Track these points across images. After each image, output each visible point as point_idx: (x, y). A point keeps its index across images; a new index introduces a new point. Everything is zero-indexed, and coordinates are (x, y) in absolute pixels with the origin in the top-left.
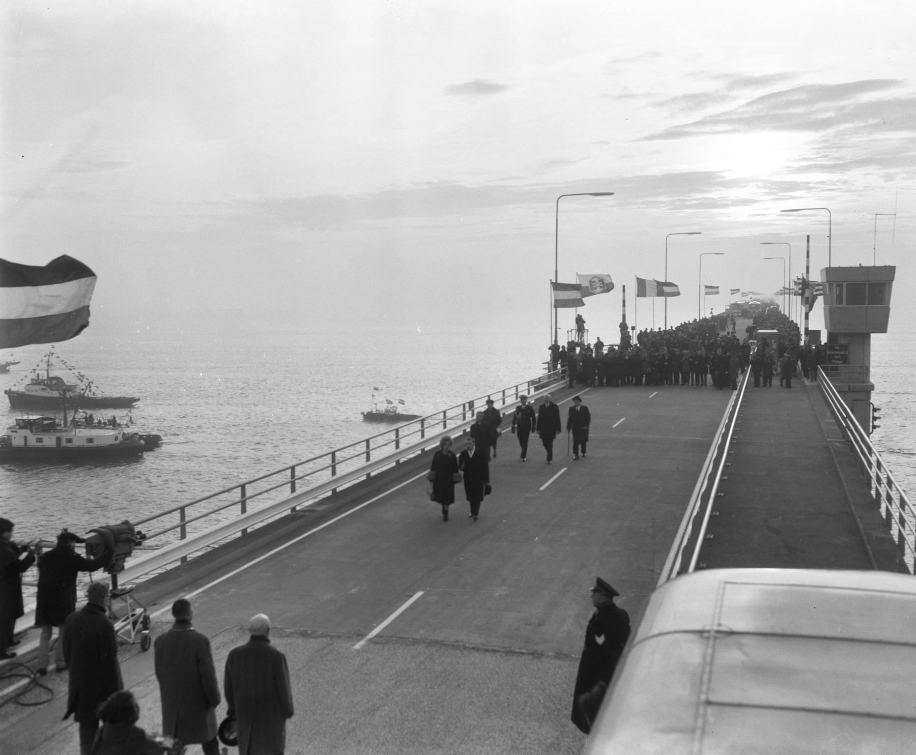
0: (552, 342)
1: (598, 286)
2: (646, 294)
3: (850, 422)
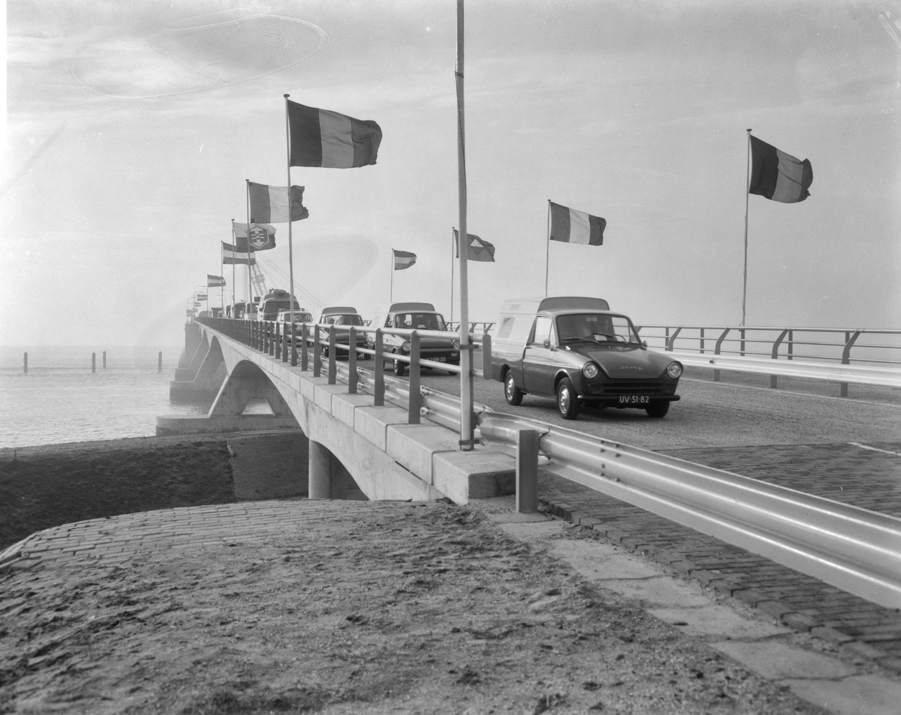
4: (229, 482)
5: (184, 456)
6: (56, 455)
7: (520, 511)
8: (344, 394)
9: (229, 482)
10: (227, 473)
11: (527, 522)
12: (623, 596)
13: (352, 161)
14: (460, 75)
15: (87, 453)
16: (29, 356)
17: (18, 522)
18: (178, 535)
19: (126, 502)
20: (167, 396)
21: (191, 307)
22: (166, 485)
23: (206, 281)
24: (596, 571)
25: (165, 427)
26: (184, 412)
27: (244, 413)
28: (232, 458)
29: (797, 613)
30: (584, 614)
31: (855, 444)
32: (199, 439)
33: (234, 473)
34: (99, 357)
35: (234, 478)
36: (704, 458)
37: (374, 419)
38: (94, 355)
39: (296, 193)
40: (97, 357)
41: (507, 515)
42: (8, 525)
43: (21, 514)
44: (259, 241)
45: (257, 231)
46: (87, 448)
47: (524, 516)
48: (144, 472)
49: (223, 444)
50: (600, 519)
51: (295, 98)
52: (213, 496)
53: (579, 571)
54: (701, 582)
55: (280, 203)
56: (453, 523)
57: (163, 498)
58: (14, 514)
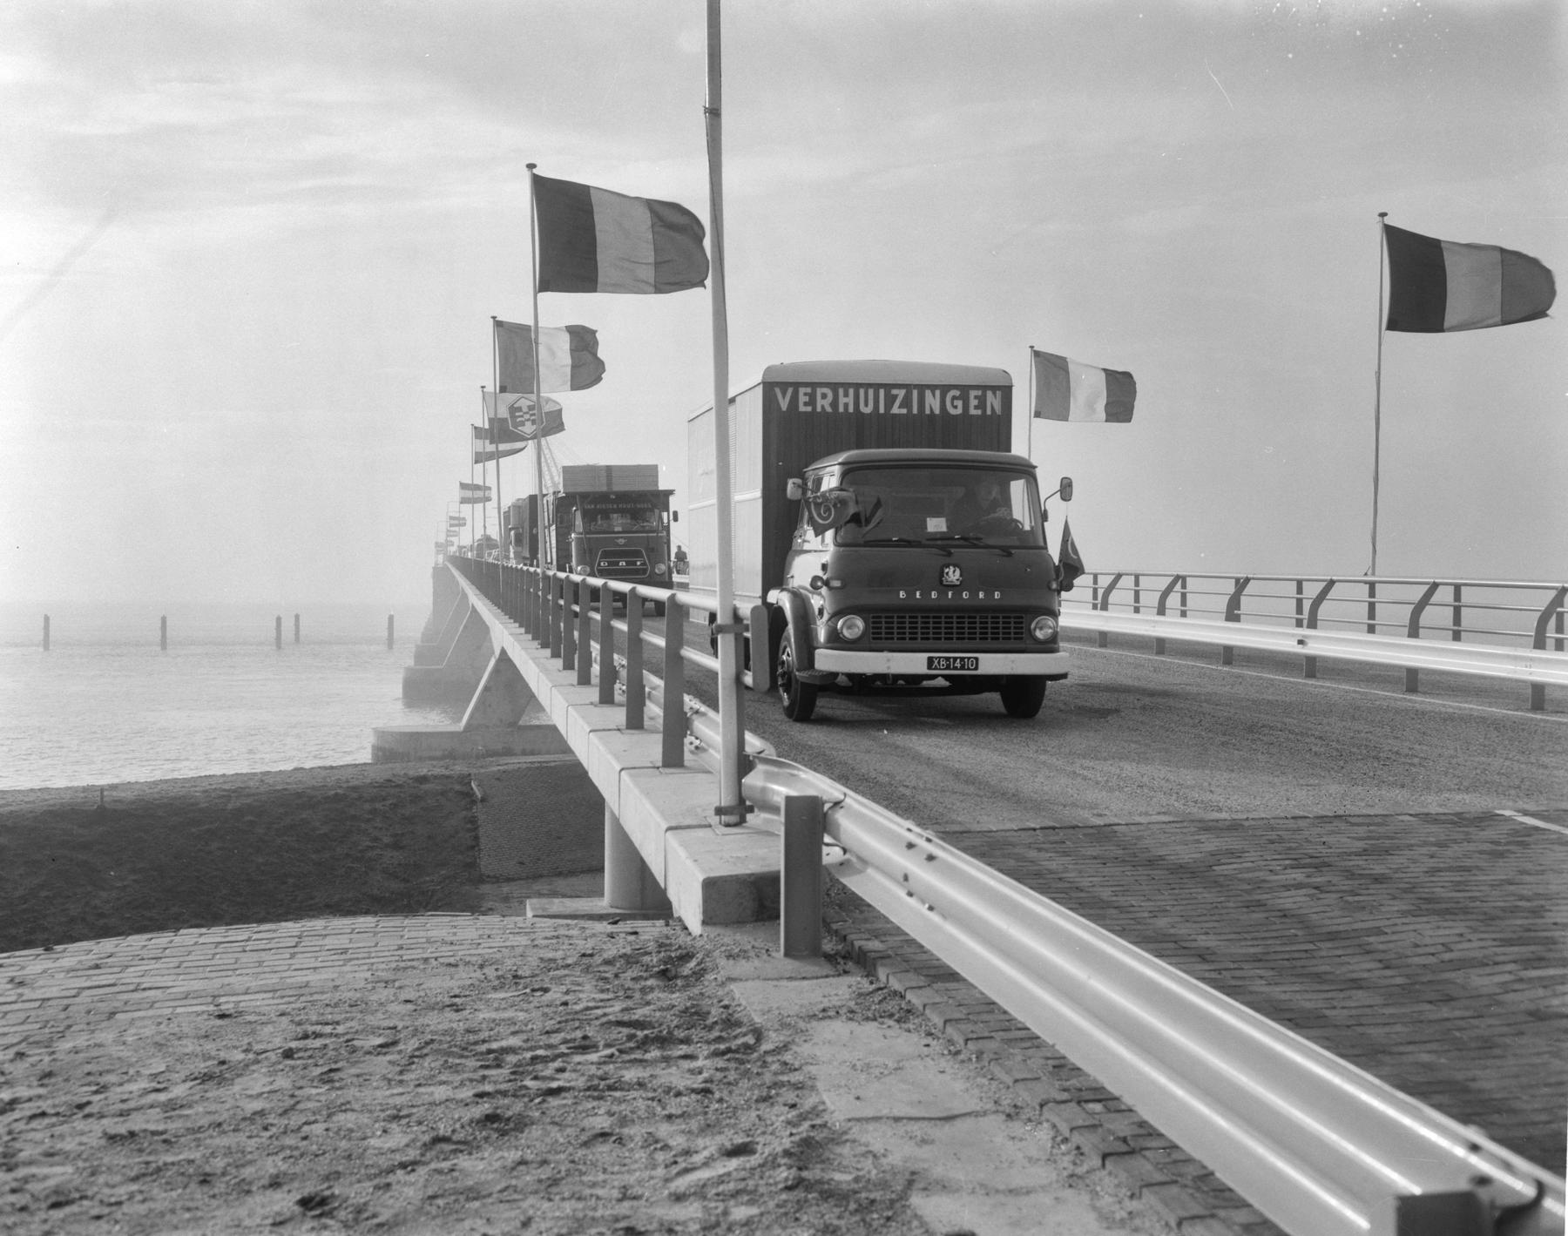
1: (528, 420)
4: (473, 847)
5: (395, 801)
6: (175, 798)
7: (787, 954)
8: (592, 704)
9: (473, 847)
10: (469, 830)
11: (790, 979)
12: (884, 1161)
13: (1495, 308)
14: (714, 113)
15: (228, 795)
16: (168, 623)
17: (102, 915)
18: (144, 989)
19: (291, 881)
20: (398, 690)
21: (442, 539)
22: (360, 851)
23: (457, 493)
24: (858, 1098)
25: (387, 746)
26: (432, 721)
27: (521, 723)
28: (480, 805)
29: (1213, 1216)
30: (771, 1204)
31: (1507, 813)
32: (424, 772)
33: (481, 831)
34: (288, 625)
35: (482, 840)
36: (1198, 841)
37: (609, 757)
38: (279, 620)
39: (583, 340)
40: (284, 624)
41: (757, 962)
42: (83, 919)
43: (108, 902)
44: (528, 424)
45: (524, 404)
46: (226, 787)
47: (791, 965)
48: (325, 829)
49: (465, 780)
50: (927, 976)
51: (542, 171)
52: (443, 872)
53: (825, 1097)
54: (1058, 1131)
55: (555, 356)
56: (651, 976)
57: (355, 875)
58: (97, 902)
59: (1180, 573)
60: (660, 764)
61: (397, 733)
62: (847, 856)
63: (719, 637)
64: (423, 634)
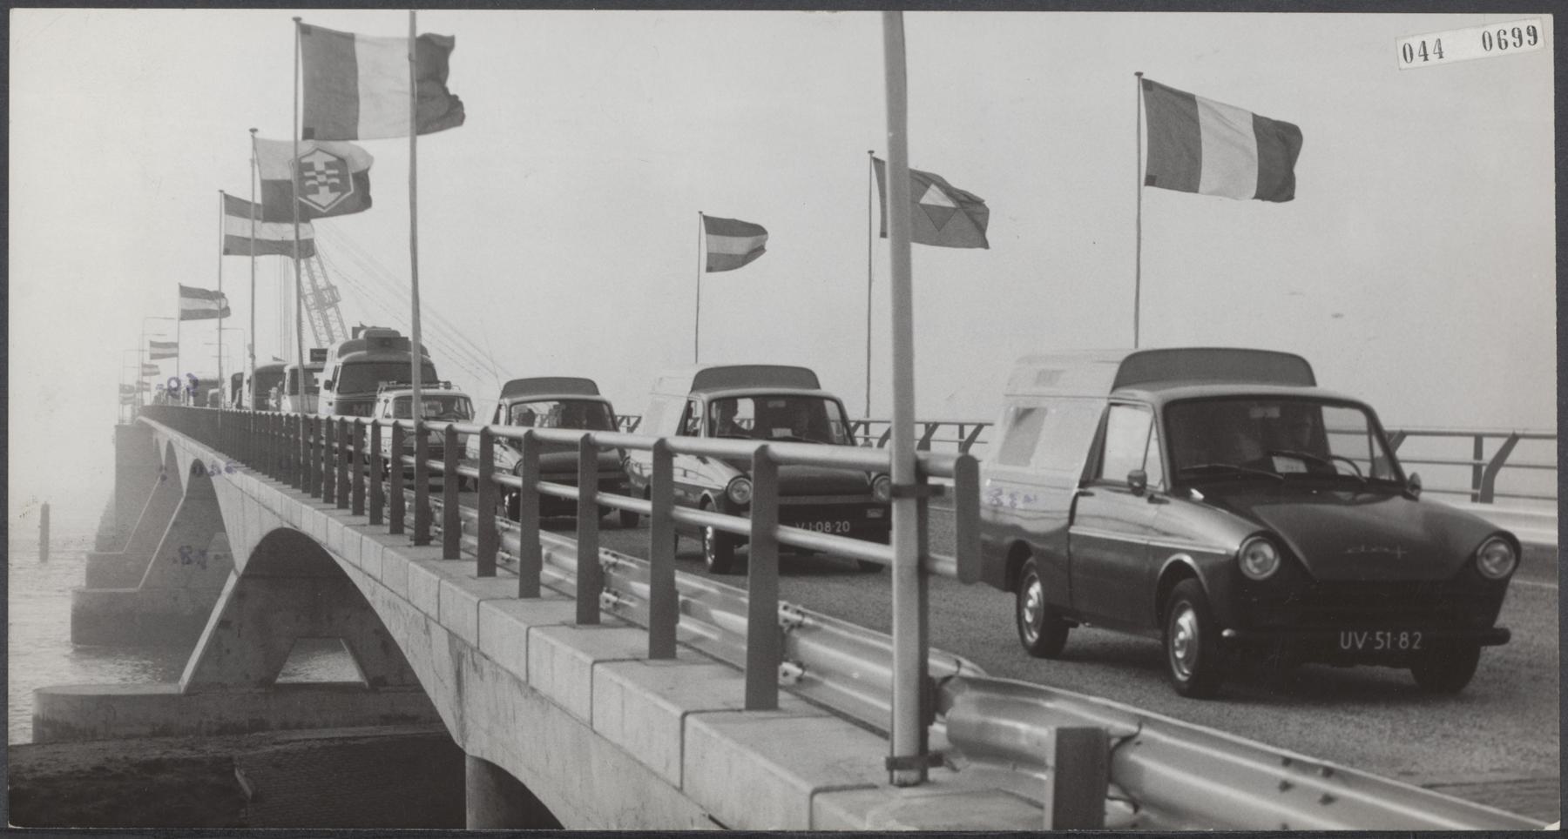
0: (320, 263)
1: (324, 184)
2: (1198, 185)
3: (1461, 805)
8: (563, 624)
20: (65, 631)
23: (174, 304)
44: (324, 190)
49: (224, 767)
59: (626, 414)
60: (742, 706)
61: (74, 697)
62: (1143, 812)
63: (894, 506)
64: (99, 537)
